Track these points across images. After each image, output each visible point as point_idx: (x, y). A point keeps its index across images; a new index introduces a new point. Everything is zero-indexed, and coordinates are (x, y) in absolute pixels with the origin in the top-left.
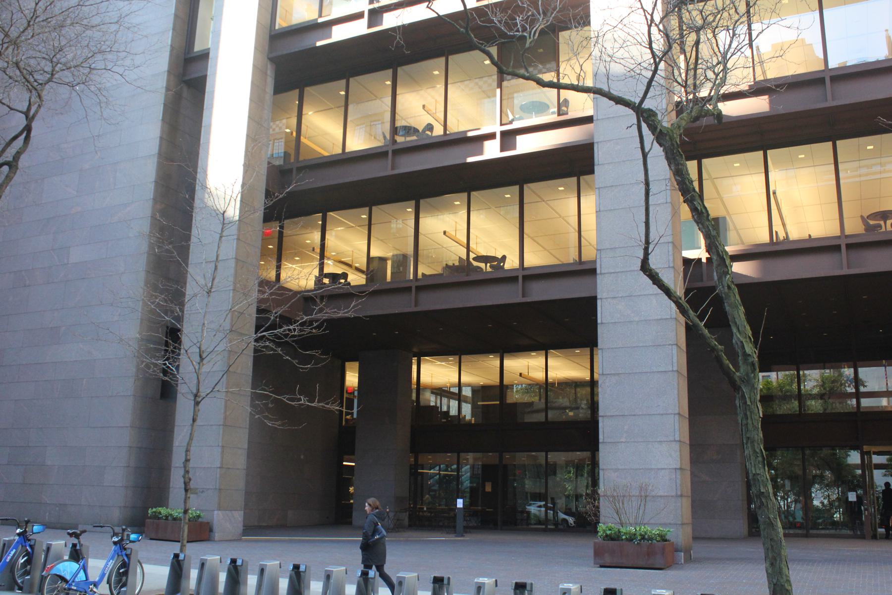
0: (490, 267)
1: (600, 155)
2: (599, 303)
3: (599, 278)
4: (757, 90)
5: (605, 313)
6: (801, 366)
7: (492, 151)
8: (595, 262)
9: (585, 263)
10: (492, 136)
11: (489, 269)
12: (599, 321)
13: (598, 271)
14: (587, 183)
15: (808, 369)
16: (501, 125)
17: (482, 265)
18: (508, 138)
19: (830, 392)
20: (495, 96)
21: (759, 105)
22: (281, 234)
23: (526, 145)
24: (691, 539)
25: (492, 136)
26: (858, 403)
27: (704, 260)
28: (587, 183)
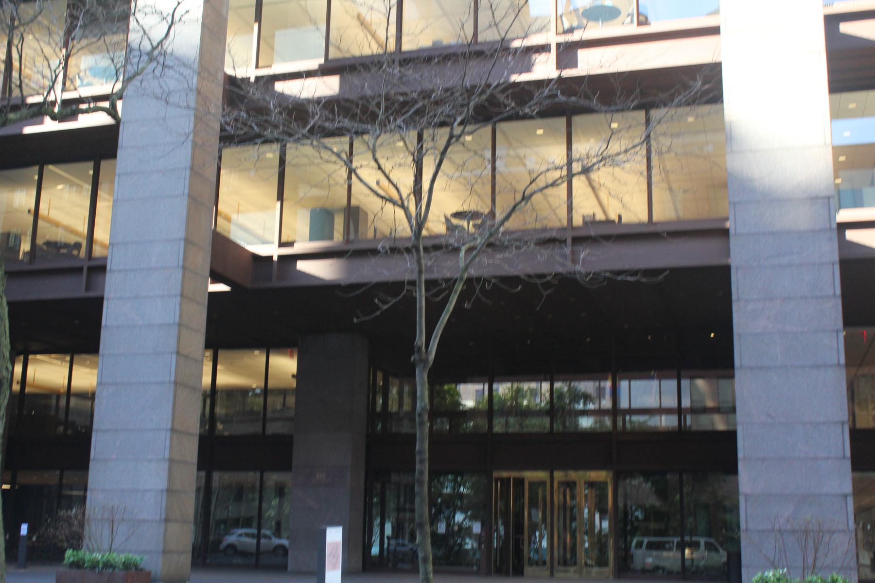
0: (474, 226)
1: (125, 137)
2: (733, 271)
3: (108, 276)
4: (325, 71)
5: (110, 315)
6: (682, 373)
7: (544, 68)
8: (106, 258)
9: (657, 224)
10: (543, 48)
11: (472, 230)
12: (103, 323)
13: (108, 268)
14: (504, 133)
15: (576, 380)
16: (257, 67)
17: (465, 224)
18: (567, 53)
19: (556, 409)
20: (252, 29)
21: (330, 86)
22: (282, 162)
23: (591, 63)
24: (186, 559)
25: (543, 48)
26: (614, 422)
27: (275, 258)
28: (504, 133)
